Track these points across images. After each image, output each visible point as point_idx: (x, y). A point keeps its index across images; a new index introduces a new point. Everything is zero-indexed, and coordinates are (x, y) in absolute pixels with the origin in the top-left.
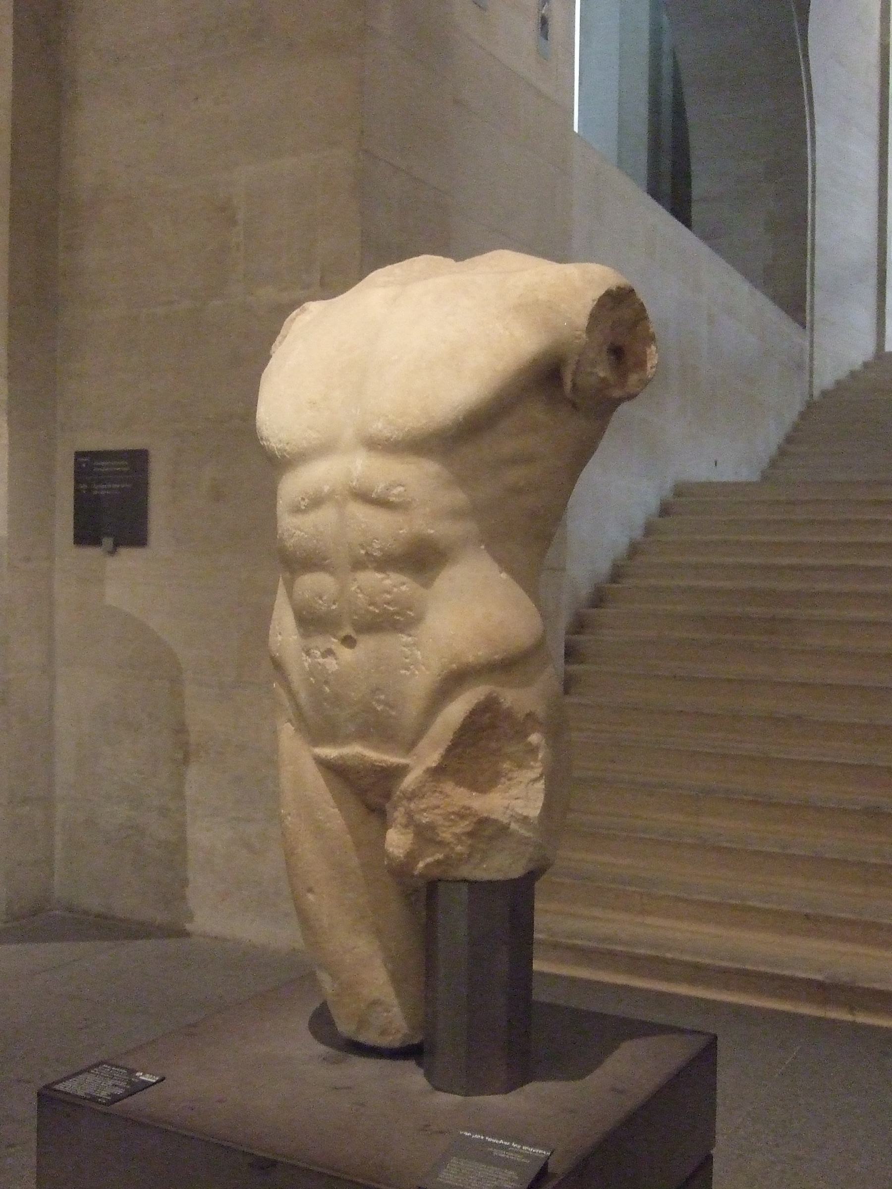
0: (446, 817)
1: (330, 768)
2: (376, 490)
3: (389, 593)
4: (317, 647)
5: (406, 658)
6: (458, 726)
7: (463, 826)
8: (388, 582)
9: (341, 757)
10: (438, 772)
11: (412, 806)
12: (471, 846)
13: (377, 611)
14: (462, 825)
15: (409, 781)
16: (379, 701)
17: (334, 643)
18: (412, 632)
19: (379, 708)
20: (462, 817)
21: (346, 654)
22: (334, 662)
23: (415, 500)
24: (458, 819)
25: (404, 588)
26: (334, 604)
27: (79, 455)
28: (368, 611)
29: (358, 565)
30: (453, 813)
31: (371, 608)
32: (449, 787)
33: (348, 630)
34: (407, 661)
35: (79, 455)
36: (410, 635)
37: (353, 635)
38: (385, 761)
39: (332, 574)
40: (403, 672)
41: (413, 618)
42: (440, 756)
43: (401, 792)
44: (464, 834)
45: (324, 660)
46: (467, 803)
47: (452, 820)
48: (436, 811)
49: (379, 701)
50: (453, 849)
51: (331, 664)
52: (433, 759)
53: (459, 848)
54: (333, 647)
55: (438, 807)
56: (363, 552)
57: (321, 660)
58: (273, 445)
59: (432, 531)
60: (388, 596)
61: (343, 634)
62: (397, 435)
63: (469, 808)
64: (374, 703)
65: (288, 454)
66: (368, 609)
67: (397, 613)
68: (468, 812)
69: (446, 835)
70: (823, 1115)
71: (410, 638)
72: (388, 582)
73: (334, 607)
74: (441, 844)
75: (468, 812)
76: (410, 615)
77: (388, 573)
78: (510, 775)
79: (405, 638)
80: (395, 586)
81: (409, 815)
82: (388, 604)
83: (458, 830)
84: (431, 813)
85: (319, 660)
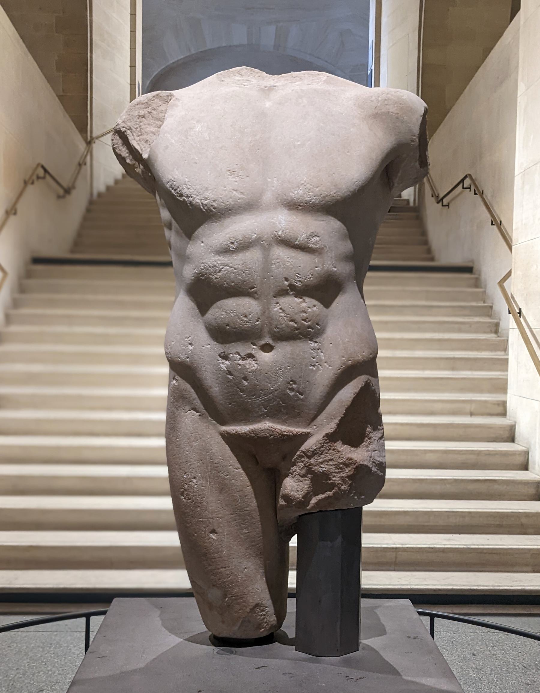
0: (337, 466)
1: (228, 438)
2: (299, 239)
3: (305, 313)
4: (237, 352)
5: (314, 358)
6: (349, 403)
7: (348, 471)
8: (304, 305)
9: (253, 431)
10: (331, 438)
11: (312, 461)
12: (351, 485)
13: (296, 325)
14: (347, 471)
15: (309, 444)
16: (292, 390)
17: (254, 350)
18: (317, 340)
19: (292, 394)
20: (347, 465)
21: (266, 357)
22: (254, 362)
23: (326, 247)
24: (344, 467)
25: (315, 308)
26: (258, 321)
27: (379, 86)
28: (288, 326)
29: (282, 293)
30: (341, 463)
31: (291, 323)
32: (339, 446)
33: (268, 340)
34: (314, 360)
35: (379, 86)
36: (316, 342)
37: (271, 342)
38: (292, 432)
39: (256, 299)
40: (311, 368)
41: (319, 330)
42: (336, 425)
43: (303, 452)
44: (348, 477)
45: (244, 362)
46: (350, 456)
47: (341, 468)
48: (331, 463)
49: (292, 390)
50: (339, 488)
51: (250, 364)
52: (331, 427)
53: (344, 487)
54: (253, 352)
55: (331, 460)
56: (286, 283)
57: (240, 362)
58: (198, 201)
59: (335, 269)
60: (305, 315)
61: (263, 342)
62: (315, 200)
63: (351, 459)
64: (288, 390)
65: (215, 208)
66: (289, 324)
67: (309, 327)
68: (351, 461)
69: (336, 479)
70: (203, 532)
71: (316, 344)
72: (304, 305)
73: (257, 323)
74: (333, 486)
75: (351, 461)
76: (317, 328)
77: (304, 298)
78: (370, 436)
79: (313, 344)
80: (309, 308)
81: (309, 470)
82: (305, 320)
83: (343, 475)
84: (327, 465)
85: (239, 362)
